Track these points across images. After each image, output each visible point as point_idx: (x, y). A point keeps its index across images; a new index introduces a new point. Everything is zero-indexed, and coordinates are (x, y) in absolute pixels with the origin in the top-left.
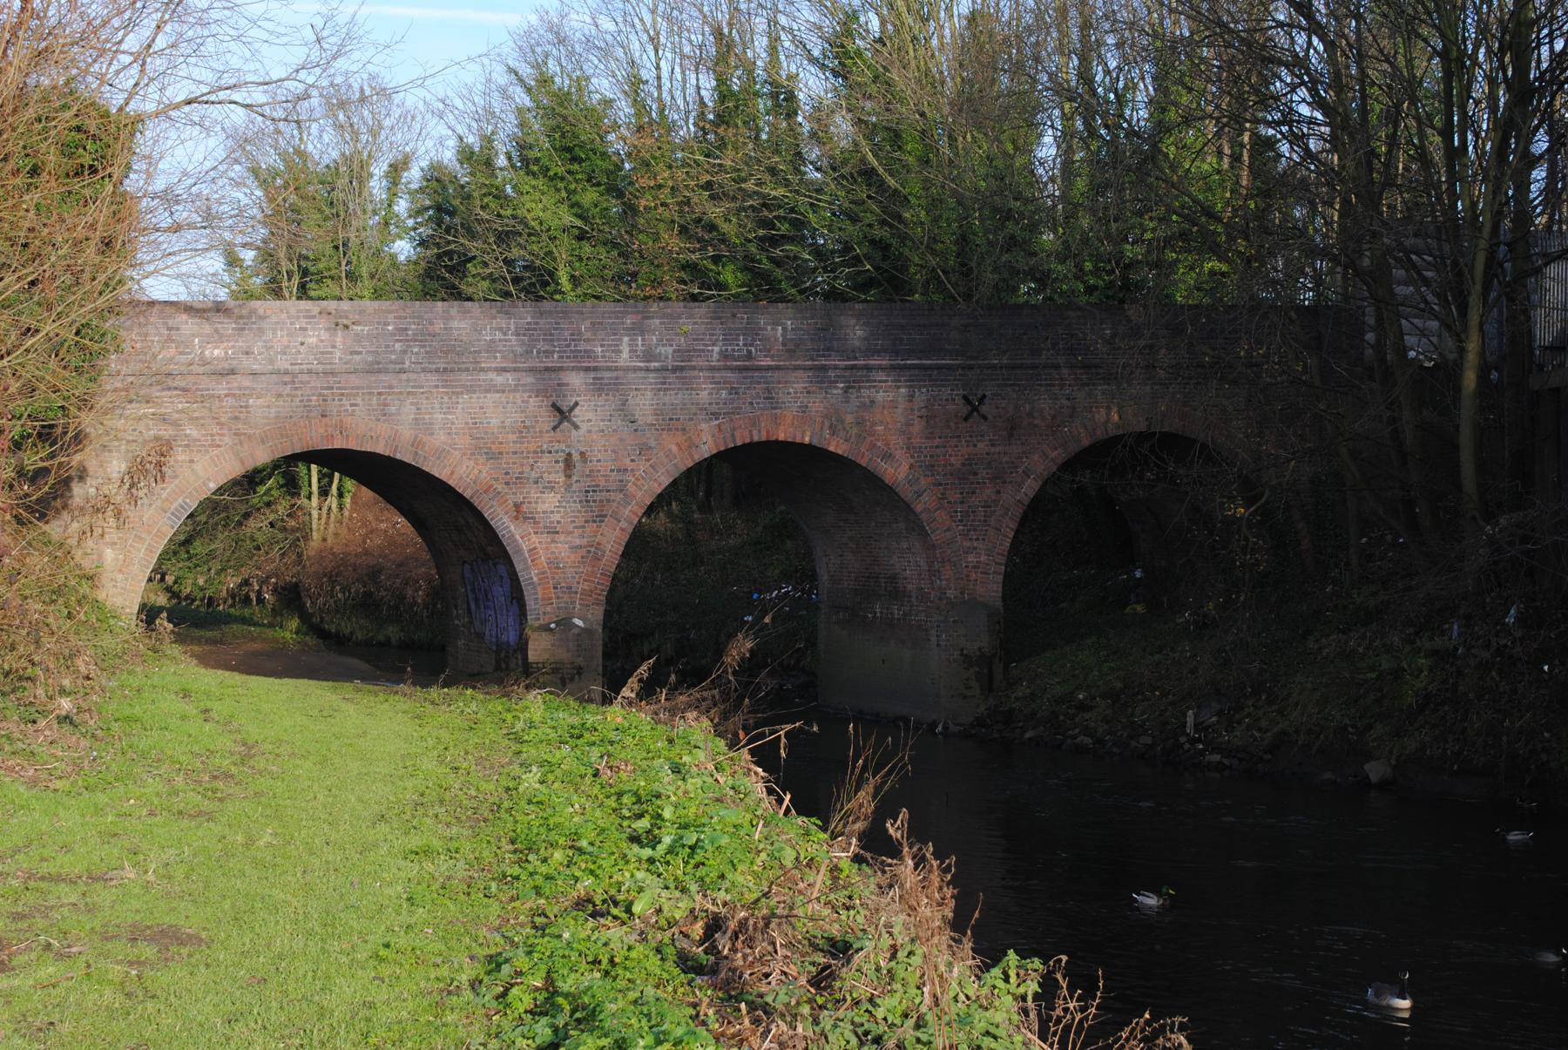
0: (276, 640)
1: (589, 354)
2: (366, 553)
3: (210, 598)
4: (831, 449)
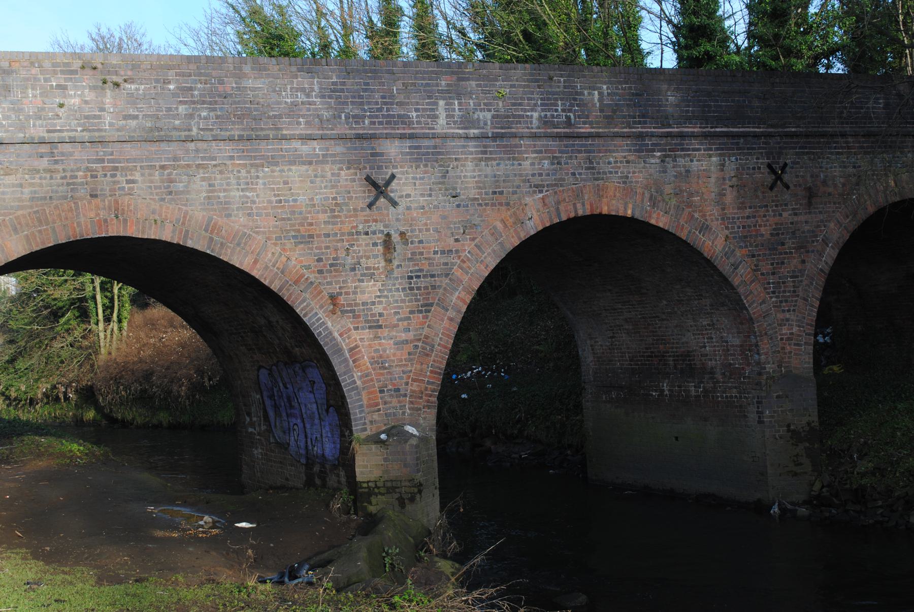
0: (62, 455)
1: (404, 120)
2: (141, 361)
3: (31, 399)
4: (653, 222)
